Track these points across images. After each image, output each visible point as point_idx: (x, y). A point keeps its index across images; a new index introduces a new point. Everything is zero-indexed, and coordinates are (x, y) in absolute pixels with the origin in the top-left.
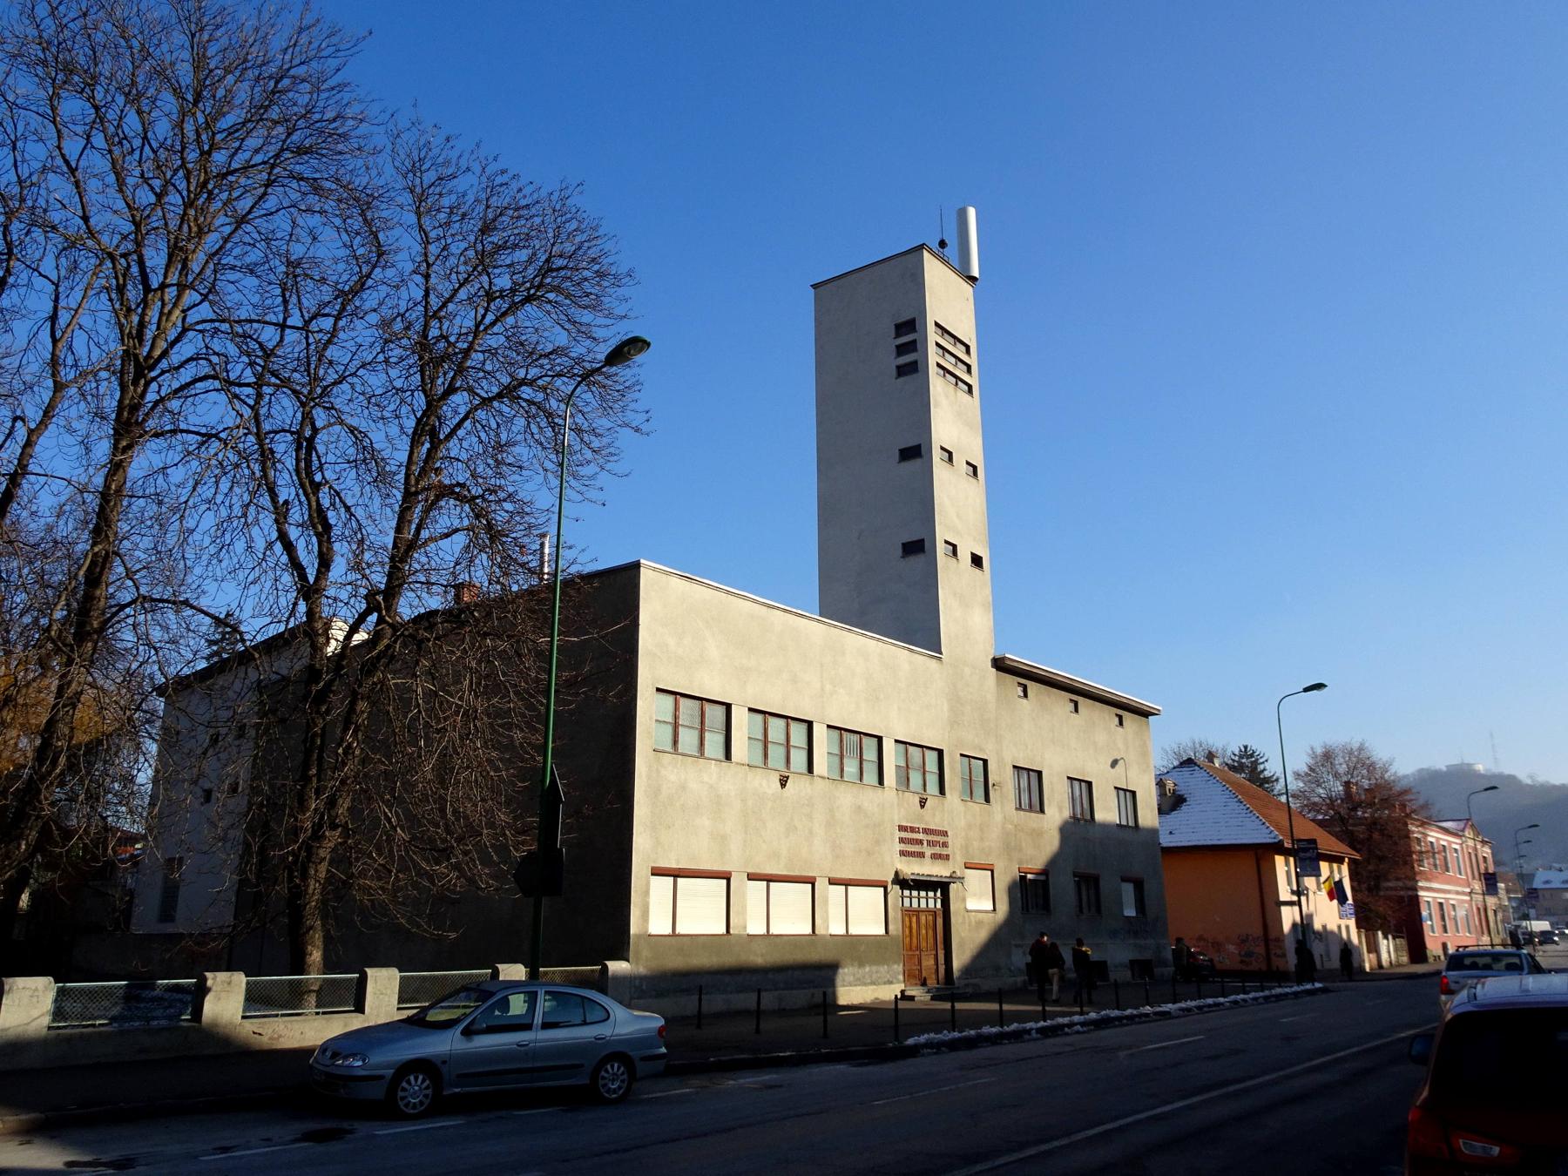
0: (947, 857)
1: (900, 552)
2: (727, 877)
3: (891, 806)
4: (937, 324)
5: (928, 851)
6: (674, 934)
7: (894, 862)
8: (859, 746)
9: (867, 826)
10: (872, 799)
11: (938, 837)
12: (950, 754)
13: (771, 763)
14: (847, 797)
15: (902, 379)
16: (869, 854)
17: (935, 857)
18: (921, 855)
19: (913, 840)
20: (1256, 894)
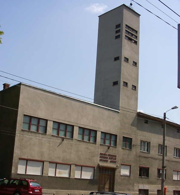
0: (116, 162)
1: (112, 84)
2: (43, 162)
3: (98, 149)
4: (126, 25)
5: (109, 160)
6: (42, 176)
7: (97, 161)
8: (89, 133)
9: (90, 152)
10: (91, 147)
11: (113, 158)
12: (119, 136)
13: (47, 133)
14: (83, 146)
15: (116, 40)
16: (89, 159)
17: (111, 162)
18: (107, 161)
19: (103, 157)
20: (71, 173)
